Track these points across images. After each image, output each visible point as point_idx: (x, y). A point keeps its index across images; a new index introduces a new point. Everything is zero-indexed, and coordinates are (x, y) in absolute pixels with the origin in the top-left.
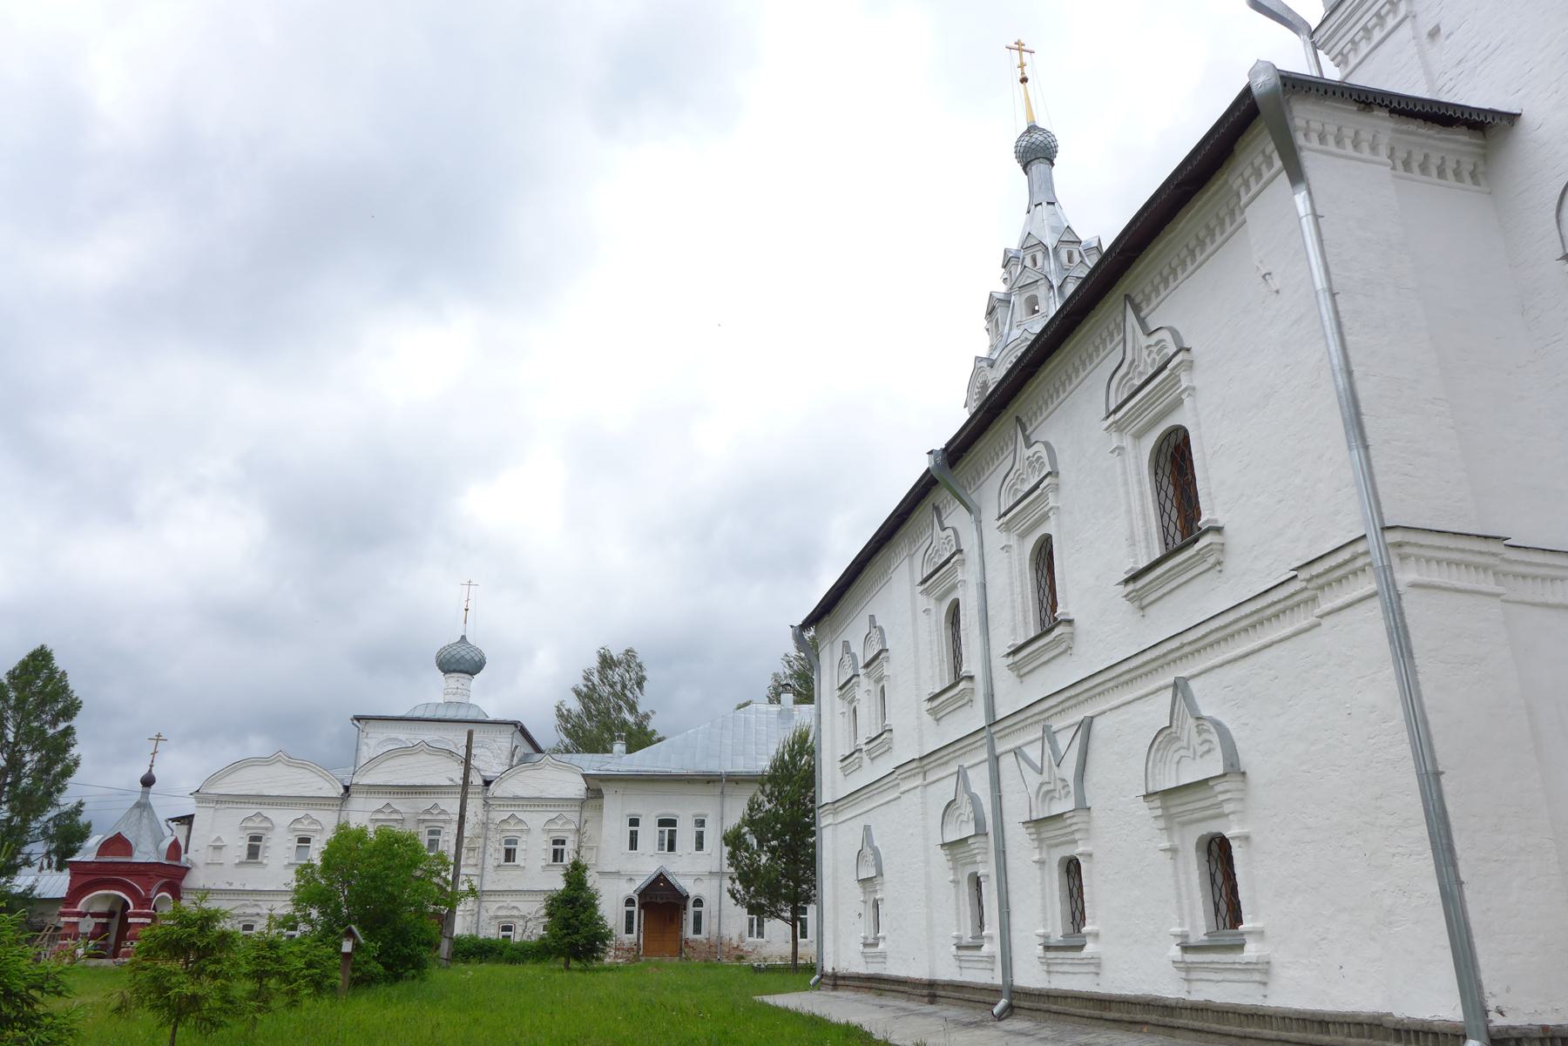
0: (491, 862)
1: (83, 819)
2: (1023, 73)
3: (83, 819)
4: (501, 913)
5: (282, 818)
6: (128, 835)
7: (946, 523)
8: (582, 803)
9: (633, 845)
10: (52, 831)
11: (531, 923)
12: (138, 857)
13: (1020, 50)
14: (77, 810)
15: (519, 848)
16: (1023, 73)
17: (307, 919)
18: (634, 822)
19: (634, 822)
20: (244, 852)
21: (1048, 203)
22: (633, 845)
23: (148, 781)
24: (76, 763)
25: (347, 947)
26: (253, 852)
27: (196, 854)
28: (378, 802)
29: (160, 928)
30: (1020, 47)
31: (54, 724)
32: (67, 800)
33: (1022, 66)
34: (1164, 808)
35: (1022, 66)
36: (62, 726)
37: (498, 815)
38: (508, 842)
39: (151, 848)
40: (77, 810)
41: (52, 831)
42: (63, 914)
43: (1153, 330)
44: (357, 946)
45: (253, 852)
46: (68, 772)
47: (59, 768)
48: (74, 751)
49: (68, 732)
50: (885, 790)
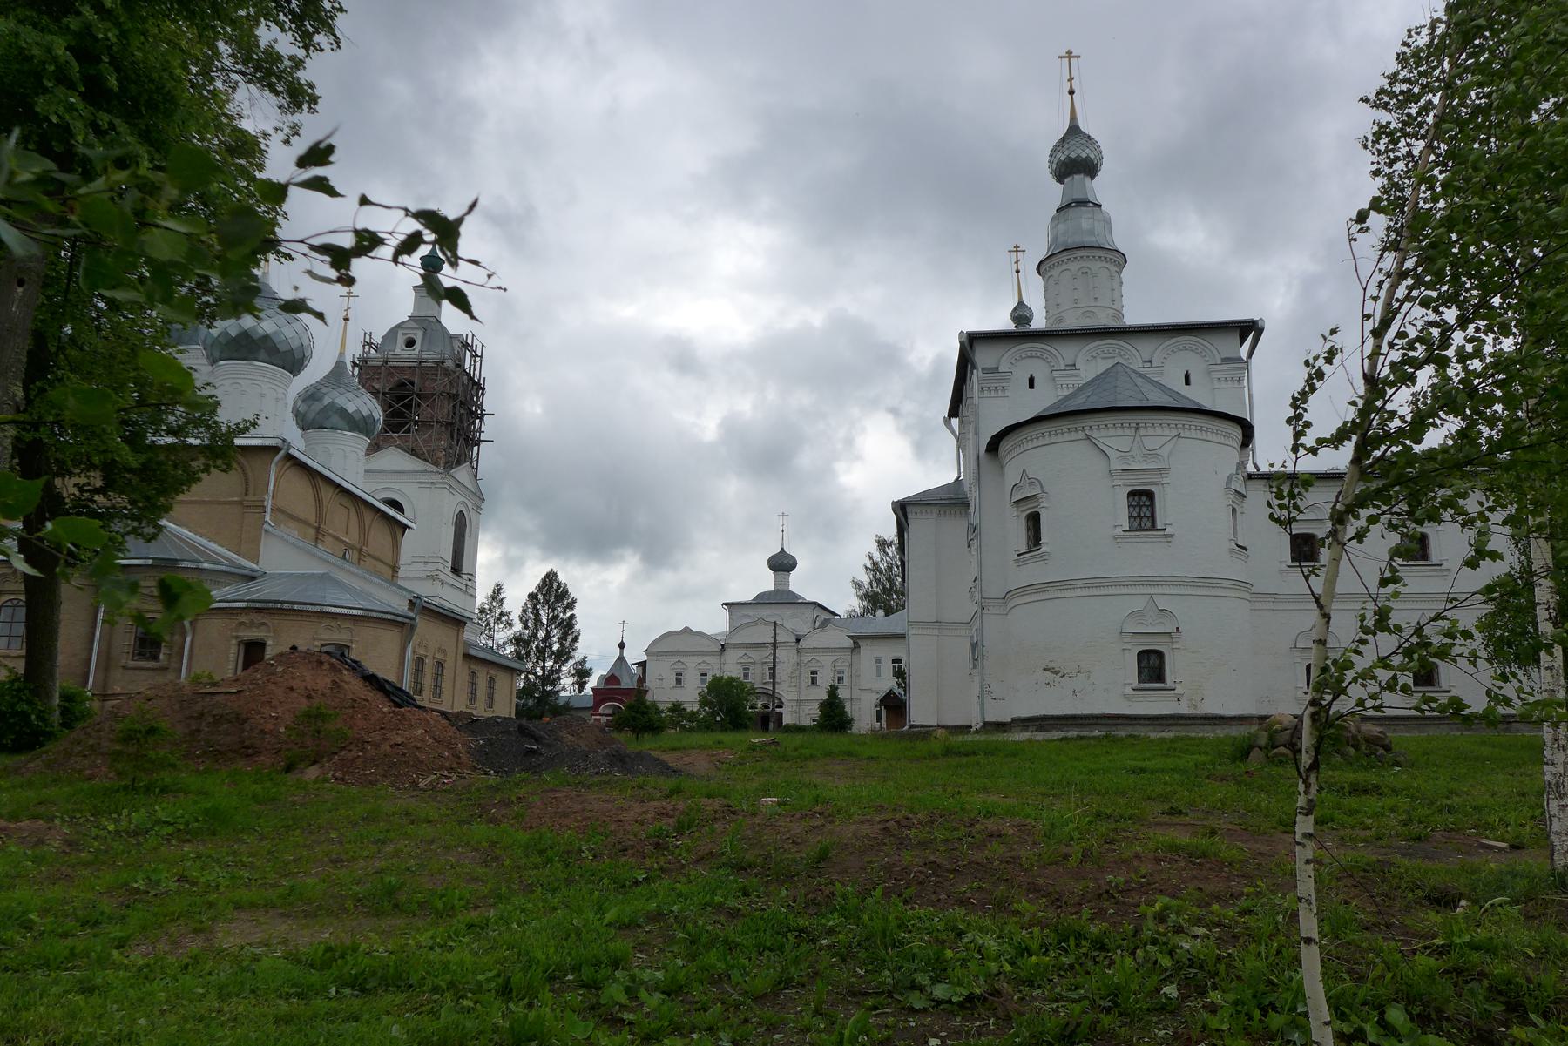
0: (803, 685)
1: (587, 666)
2: (1071, 87)
3: (587, 666)
4: (811, 712)
5: (691, 663)
6: (617, 674)
8: (852, 650)
9: (879, 675)
10: (573, 672)
11: (808, 714)
12: (623, 686)
13: (1017, 251)
14: (584, 661)
15: (818, 676)
16: (1071, 87)
17: (704, 711)
18: (878, 661)
19: (878, 661)
20: (674, 682)
22: (879, 675)
23: (622, 646)
24: (579, 634)
25: (718, 719)
26: (679, 681)
27: (650, 683)
28: (741, 653)
29: (1052, 980)
31: (565, 613)
32: (578, 655)
33: (1017, 262)
35: (1017, 262)
36: (568, 614)
37: (805, 658)
38: (812, 673)
39: (629, 681)
40: (584, 661)
41: (573, 672)
42: (592, 715)
43: (1132, 319)
44: (722, 719)
45: (679, 681)
46: (575, 639)
47: (571, 637)
48: (577, 627)
49: (572, 617)
50: (320, 558)
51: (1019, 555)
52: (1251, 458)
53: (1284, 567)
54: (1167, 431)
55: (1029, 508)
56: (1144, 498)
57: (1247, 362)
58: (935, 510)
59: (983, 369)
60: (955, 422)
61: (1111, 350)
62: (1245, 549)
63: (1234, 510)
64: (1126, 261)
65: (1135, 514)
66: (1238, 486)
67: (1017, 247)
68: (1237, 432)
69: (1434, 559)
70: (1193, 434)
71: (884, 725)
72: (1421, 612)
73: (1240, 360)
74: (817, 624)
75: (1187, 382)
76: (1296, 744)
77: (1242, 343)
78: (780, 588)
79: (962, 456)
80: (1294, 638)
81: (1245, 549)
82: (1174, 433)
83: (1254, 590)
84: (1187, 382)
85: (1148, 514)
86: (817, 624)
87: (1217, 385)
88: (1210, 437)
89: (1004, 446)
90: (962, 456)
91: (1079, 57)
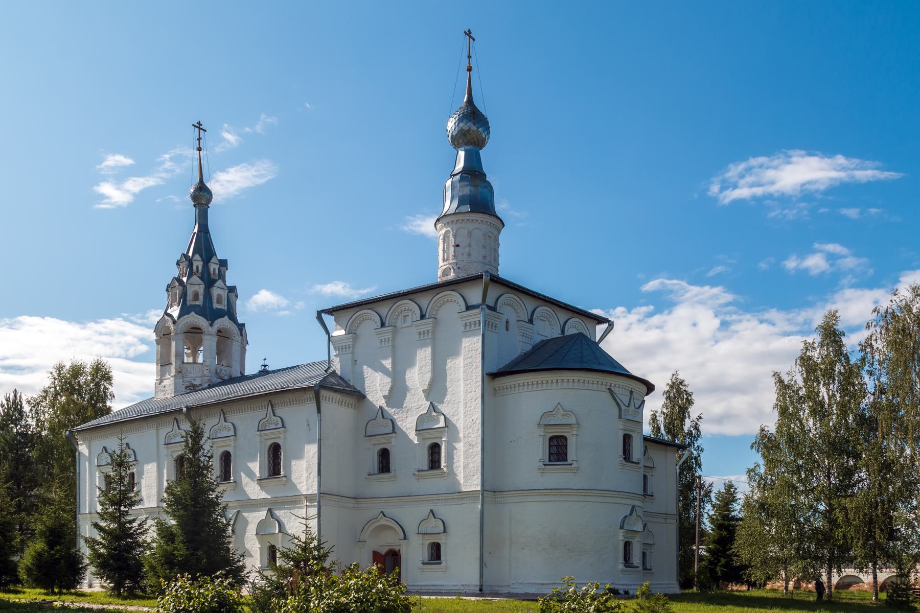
7: (181, 427)
13: (200, 128)
21: (205, 232)
30: (199, 126)
33: (199, 139)
34: (423, 537)
35: (199, 139)
67: (199, 123)
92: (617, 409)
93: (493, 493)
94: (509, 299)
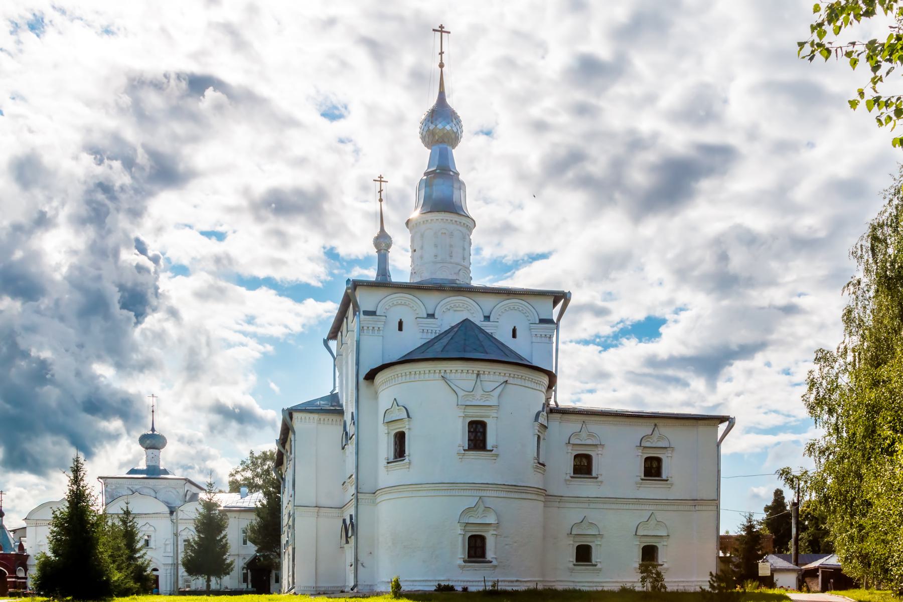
13: (381, 181)
33: (380, 191)
43: (475, 283)
51: (388, 463)
52: (553, 397)
53: (568, 477)
54: (497, 378)
55: (397, 428)
56: (479, 426)
57: (557, 324)
58: (316, 416)
59: (364, 311)
60: (333, 344)
61: (461, 305)
62: (544, 465)
63: (539, 437)
64: (475, 226)
65: (472, 438)
66: (543, 420)
67: (381, 177)
68: (545, 380)
69: (664, 477)
70: (518, 381)
71: (250, 586)
72: (651, 512)
73: (550, 321)
74: (188, 497)
75: (514, 336)
76: (844, 351)
77: (554, 306)
78: (151, 464)
79: (337, 374)
80: (572, 524)
81: (544, 465)
82: (502, 379)
83: (547, 493)
84: (514, 336)
85: (481, 438)
86: (188, 497)
87: (534, 339)
88: (528, 384)
89: (380, 378)
90: (337, 374)
91: (449, 33)
92: (456, 395)
93: (373, 495)
94: (398, 298)
